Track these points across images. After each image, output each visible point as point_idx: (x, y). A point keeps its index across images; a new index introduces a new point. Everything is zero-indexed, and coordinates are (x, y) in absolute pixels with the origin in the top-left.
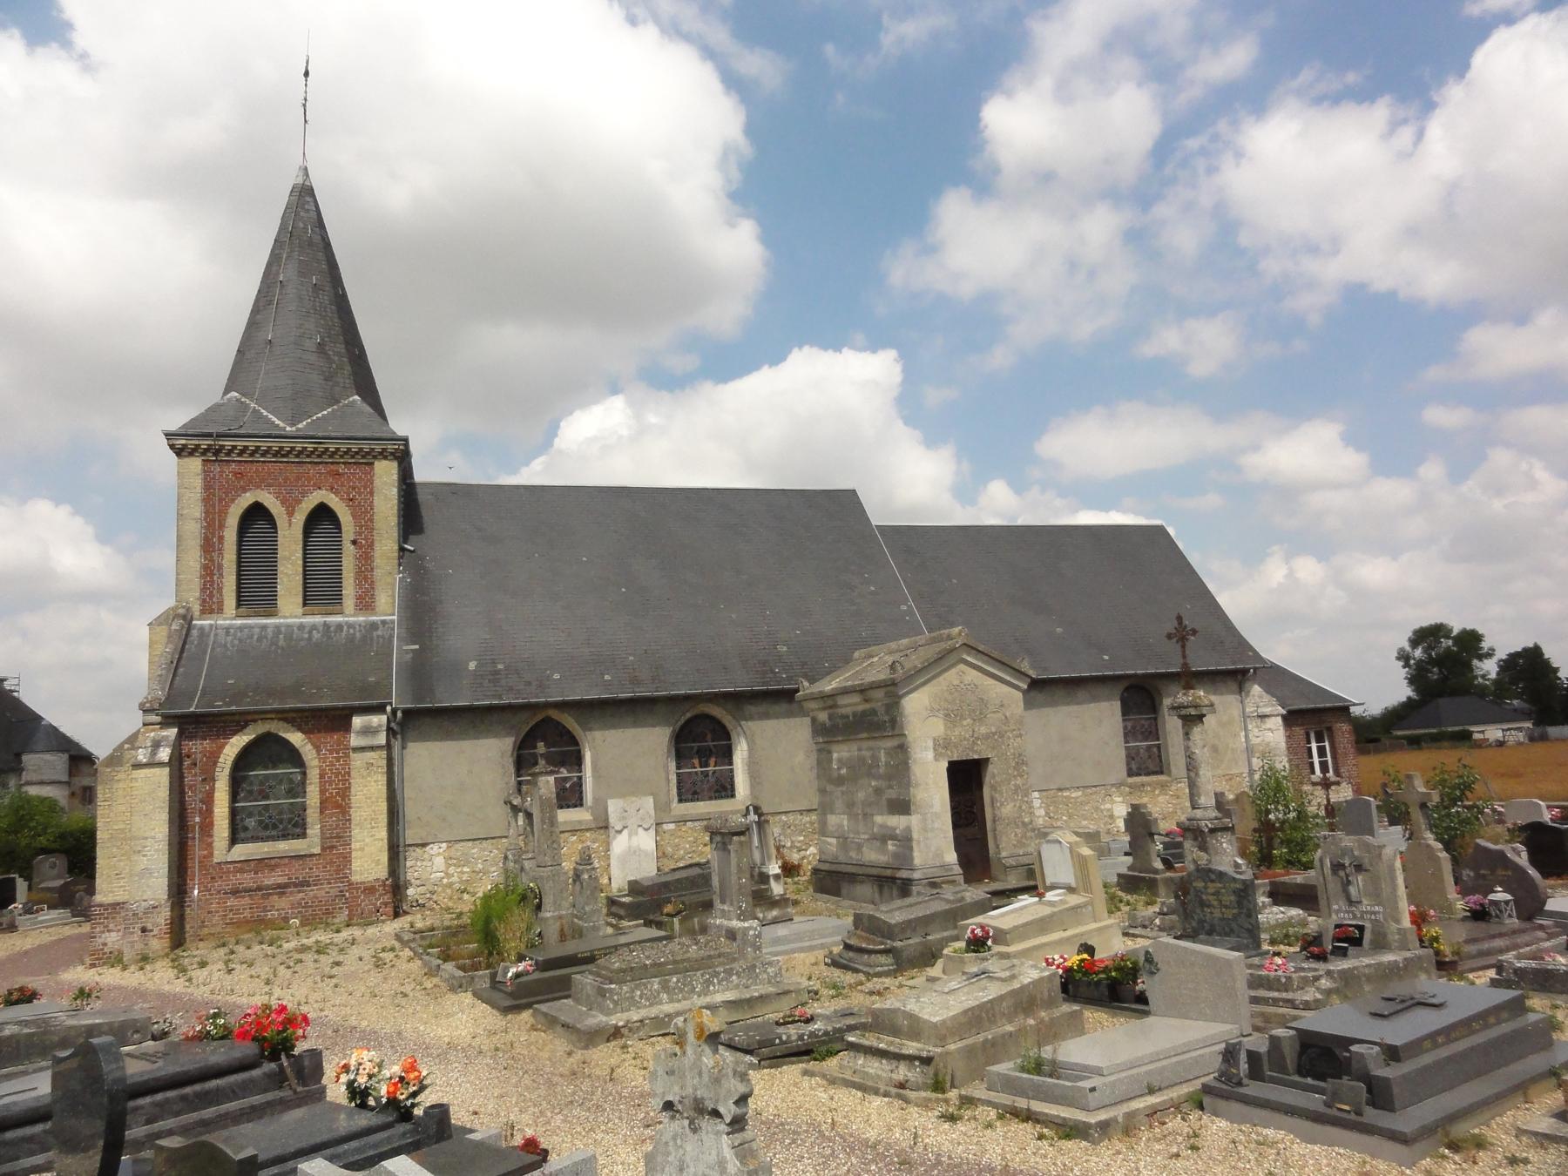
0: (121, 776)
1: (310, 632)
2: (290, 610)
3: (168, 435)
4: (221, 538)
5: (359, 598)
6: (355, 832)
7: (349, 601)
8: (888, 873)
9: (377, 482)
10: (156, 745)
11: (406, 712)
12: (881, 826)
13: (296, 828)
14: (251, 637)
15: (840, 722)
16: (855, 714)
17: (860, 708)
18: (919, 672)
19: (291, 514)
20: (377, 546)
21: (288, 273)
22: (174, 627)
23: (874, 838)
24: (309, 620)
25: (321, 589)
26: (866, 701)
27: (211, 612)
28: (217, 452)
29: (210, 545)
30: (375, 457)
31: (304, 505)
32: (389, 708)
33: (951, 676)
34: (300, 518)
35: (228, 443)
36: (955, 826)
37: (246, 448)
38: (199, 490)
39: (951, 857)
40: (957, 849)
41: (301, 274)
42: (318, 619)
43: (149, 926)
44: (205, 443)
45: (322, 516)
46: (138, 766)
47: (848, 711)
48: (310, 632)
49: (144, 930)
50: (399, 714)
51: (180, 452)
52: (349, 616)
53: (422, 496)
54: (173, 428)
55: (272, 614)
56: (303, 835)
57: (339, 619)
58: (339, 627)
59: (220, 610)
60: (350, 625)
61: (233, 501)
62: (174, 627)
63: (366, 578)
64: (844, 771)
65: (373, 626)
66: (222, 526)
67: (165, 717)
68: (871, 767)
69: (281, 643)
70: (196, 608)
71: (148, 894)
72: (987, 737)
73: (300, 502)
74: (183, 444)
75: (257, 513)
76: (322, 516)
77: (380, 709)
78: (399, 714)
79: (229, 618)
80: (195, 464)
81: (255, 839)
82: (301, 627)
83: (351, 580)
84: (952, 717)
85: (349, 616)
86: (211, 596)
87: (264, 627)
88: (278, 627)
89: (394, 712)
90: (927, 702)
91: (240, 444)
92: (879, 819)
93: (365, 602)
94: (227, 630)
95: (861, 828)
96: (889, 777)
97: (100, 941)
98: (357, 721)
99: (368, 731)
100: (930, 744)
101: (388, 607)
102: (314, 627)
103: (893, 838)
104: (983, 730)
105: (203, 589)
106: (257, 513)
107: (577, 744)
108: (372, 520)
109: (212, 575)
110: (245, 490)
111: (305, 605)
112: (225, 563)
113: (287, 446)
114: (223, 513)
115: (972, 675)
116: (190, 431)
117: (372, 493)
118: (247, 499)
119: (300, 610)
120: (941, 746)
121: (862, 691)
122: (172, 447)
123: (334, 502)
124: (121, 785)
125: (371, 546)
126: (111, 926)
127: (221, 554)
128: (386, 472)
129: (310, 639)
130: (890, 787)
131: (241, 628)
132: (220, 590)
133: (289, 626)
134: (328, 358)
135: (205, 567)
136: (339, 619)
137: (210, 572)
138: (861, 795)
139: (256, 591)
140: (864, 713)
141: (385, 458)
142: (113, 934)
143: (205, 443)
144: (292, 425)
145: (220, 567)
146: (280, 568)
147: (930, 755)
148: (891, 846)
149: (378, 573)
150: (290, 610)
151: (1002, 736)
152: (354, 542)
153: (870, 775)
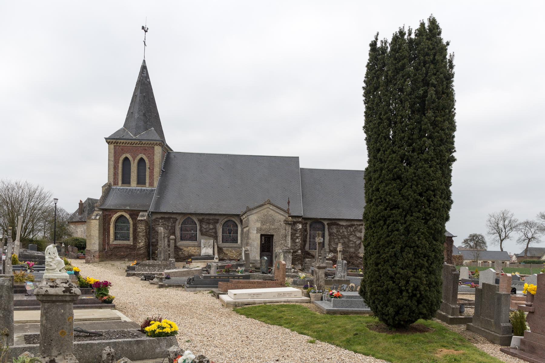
2: (134, 185)
3: (106, 138)
5: (150, 183)
6: (385, 334)
7: (147, 184)
9: (155, 152)
10: (97, 215)
11: (152, 212)
13: (128, 239)
19: (134, 160)
25: (141, 181)
28: (117, 143)
29: (116, 168)
33: (265, 212)
34: (136, 161)
35: (119, 141)
41: (141, 93)
42: (140, 188)
44: (114, 141)
45: (142, 160)
51: (108, 143)
52: (147, 187)
53: (172, 156)
54: (107, 137)
56: (129, 240)
57: (144, 188)
58: (144, 190)
59: (118, 184)
60: (147, 190)
66: (118, 163)
70: (112, 183)
72: (274, 229)
74: (109, 140)
75: (126, 159)
76: (142, 160)
81: (120, 240)
84: (263, 223)
85: (147, 187)
87: (127, 189)
90: (256, 218)
91: (122, 141)
93: (151, 184)
98: (141, 213)
99: (143, 216)
102: (138, 190)
104: (273, 227)
105: (114, 179)
106: (126, 159)
113: (133, 142)
114: (119, 160)
118: (124, 156)
120: (258, 230)
123: (144, 157)
125: (153, 169)
128: (158, 150)
133: (133, 189)
134: (146, 117)
135: (114, 173)
136: (144, 188)
137: (115, 174)
139: (126, 180)
143: (114, 141)
147: (255, 232)
150: (134, 185)
151: (279, 229)
152: (149, 168)
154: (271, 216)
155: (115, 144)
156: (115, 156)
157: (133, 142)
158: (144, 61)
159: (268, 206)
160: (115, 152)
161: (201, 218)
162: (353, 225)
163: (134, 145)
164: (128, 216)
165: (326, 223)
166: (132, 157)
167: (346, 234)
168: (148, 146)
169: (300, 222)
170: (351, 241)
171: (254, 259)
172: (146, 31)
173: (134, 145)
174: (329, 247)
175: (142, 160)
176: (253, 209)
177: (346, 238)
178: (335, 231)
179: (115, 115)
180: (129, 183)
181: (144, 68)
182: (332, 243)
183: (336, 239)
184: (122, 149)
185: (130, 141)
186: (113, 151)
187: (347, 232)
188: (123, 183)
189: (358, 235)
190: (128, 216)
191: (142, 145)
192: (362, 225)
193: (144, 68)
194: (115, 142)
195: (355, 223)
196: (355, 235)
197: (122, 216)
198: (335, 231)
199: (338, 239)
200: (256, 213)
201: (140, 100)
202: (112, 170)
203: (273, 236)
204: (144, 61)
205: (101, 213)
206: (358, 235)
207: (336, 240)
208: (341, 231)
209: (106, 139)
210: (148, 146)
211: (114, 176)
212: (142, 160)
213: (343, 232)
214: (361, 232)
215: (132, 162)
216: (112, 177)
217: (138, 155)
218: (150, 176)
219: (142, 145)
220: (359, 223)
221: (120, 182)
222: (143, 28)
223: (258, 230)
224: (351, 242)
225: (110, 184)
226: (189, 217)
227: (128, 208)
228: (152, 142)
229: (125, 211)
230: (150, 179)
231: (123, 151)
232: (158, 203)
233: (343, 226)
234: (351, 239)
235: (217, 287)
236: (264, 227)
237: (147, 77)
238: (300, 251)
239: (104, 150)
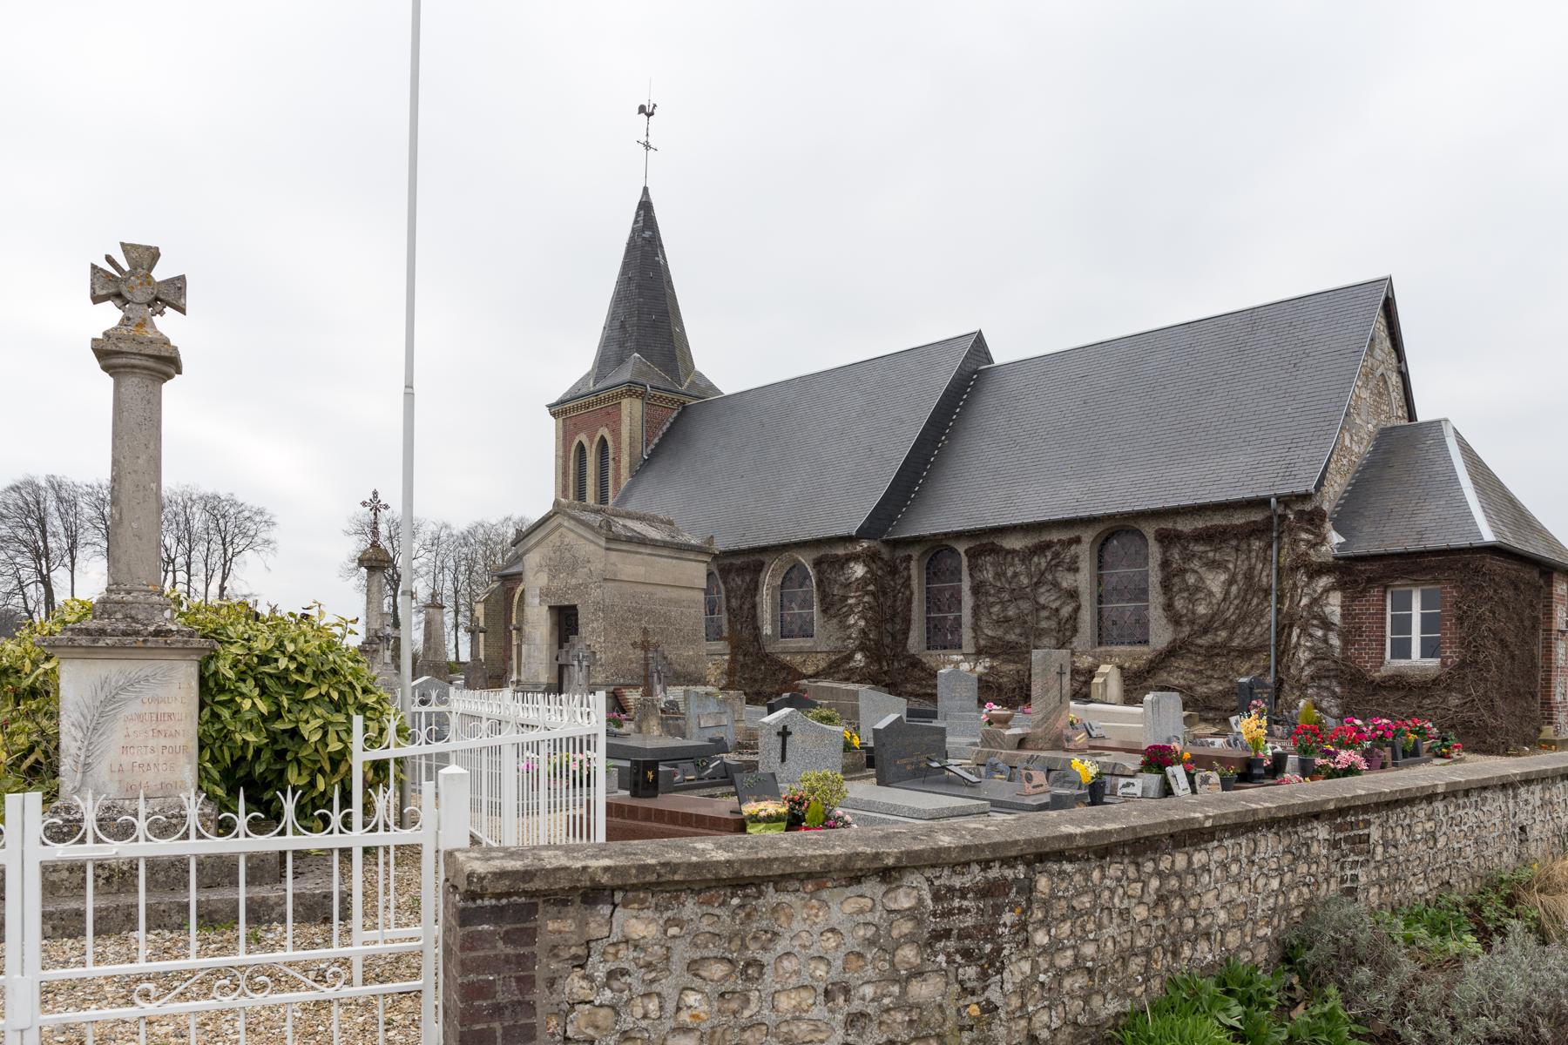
29: (565, 474)
33: (554, 538)
45: (603, 441)
51: (553, 414)
76: (603, 441)
104: (574, 582)
147: (537, 601)
158: (646, 190)
162: (1049, 545)
165: (961, 548)
167: (1026, 581)
169: (855, 558)
170: (1044, 607)
172: (650, 115)
174: (976, 638)
177: (1024, 597)
178: (988, 575)
179: (573, 355)
181: (645, 207)
182: (984, 621)
183: (993, 604)
187: (1030, 576)
189: (1067, 581)
192: (1078, 541)
193: (645, 207)
195: (1055, 536)
196: (1056, 585)
198: (988, 575)
199: (1002, 602)
200: (537, 544)
203: (574, 607)
204: (646, 190)
206: (1067, 581)
207: (995, 609)
208: (1009, 573)
213: (1016, 575)
214: (1077, 570)
220: (1065, 535)
222: (642, 109)
223: (545, 594)
224: (1044, 614)
233: (1013, 552)
234: (1042, 600)
238: (858, 656)
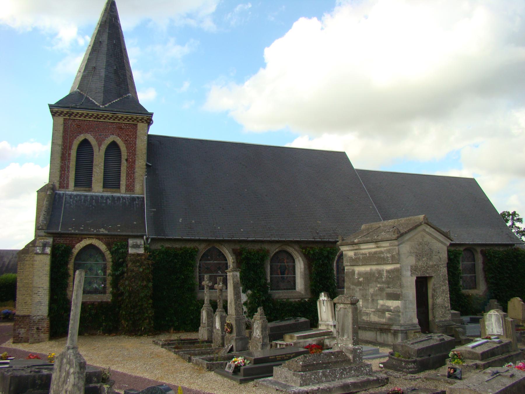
0: (28, 258)
1: (106, 200)
2: (97, 189)
4: (69, 154)
5: (127, 186)
7: (123, 188)
8: (386, 327)
9: (138, 133)
11: (153, 239)
12: (382, 306)
14: (81, 200)
15: (361, 256)
16: (369, 253)
17: (374, 250)
18: (406, 233)
19: (100, 145)
20: (137, 162)
21: (105, 38)
22: (48, 193)
23: (378, 311)
24: (106, 194)
25: (111, 181)
26: (378, 247)
27: (63, 188)
28: (71, 115)
30: (138, 121)
31: (106, 142)
32: (145, 237)
34: (104, 147)
35: (75, 111)
36: (418, 307)
37: (83, 113)
38: (61, 132)
39: (416, 321)
40: (418, 318)
43: (40, 327)
44: (66, 110)
45: (113, 146)
46: (37, 254)
47: (366, 251)
48: (106, 200)
49: (38, 329)
50: (149, 240)
52: (122, 193)
55: (89, 191)
58: (119, 198)
59: (67, 187)
60: (124, 198)
61: (75, 138)
62: (48, 193)
63: (131, 177)
64: (361, 279)
65: (133, 199)
66: (70, 148)
67: (48, 233)
68: (377, 278)
69: (94, 204)
70: (57, 185)
71: (40, 313)
72: (433, 266)
73: (104, 140)
75: (85, 143)
77: (141, 237)
78: (149, 240)
79: (71, 190)
80: (61, 119)
82: (102, 197)
83: (125, 178)
84: (419, 256)
86: (64, 181)
87: (86, 196)
88: (92, 196)
89: (147, 239)
92: (381, 302)
93: (130, 188)
94: (71, 196)
95: (370, 305)
96: (388, 283)
97: (17, 332)
99: (136, 246)
100: (409, 268)
101: (140, 189)
102: (108, 198)
103: (389, 310)
104: (431, 263)
106: (85, 143)
107: (226, 260)
108: (135, 150)
109: (65, 171)
110: (81, 133)
111: (104, 187)
112: (71, 166)
113: (100, 113)
114: (71, 144)
115: (428, 238)
116: (60, 105)
117: (136, 138)
118: (81, 137)
119: (102, 189)
120: (414, 269)
121: (402, 235)
122: (52, 112)
123: (119, 141)
124: (27, 262)
125: (134, 162)
126: (22, 326)
127: (69, 162)
129: (106, 202)
130: (388, 287)
131: (76, 196)
132: (68, 177)
133: (96, 196)
136: (118, 195)
138: (371, 291)
139: (84, 179)
140: (375, 253)
141: (143, 122)
142: (23, 330)
143: (66, 110)
144: (103, 105)
145: (68, 167)
146: (94, 170)
147: (409, 273)
148: (387, 314)
149: (137, 175)
150: (97, 189)
151: (438, 267)
152: (127, 160)
153: (376, 281)
154: (428, 244)
155: (67, 117)
156: (64, 138)
157: (100, 113)
159: (424, 227)
160: (65, 131)
161: (238, 247)
163: (102, 120)
164: (103, 247)
166: (97, 140)
168: (126, 122)
171: (410, 323)
173: (102, 120)
175: (114, 145)
176: (406, 233)
180: (89, 185)
184: (79, 126)
185: (95, 113)
186: (61, 128)
188: (77, 184)
190: (103, 247)
191: (116, 121)
194: (68, 113)
197: (91, 247)
200: (408, 240)
201: (108, 49)
202: (58, 161)
205: (50, 240)
209: (51, 106)
210: (126, 122)
211: (61, 171)
212: (114, 145)
215: (96, 149)
216: (58, 174)
217: (107, 136)
218: (128, 174)
219: (116, 121)
221: (72, 183)
225: (54, 186)
226: (214, 247)
227: (103, 231)
228: (135, 116)
229: (98, 236)
230: (127, 179)
231: (80, 128)
232: (158, 222)
235: (272, 376)
236: (420, 263)
237: (116, 18)
239: (46, 124)
